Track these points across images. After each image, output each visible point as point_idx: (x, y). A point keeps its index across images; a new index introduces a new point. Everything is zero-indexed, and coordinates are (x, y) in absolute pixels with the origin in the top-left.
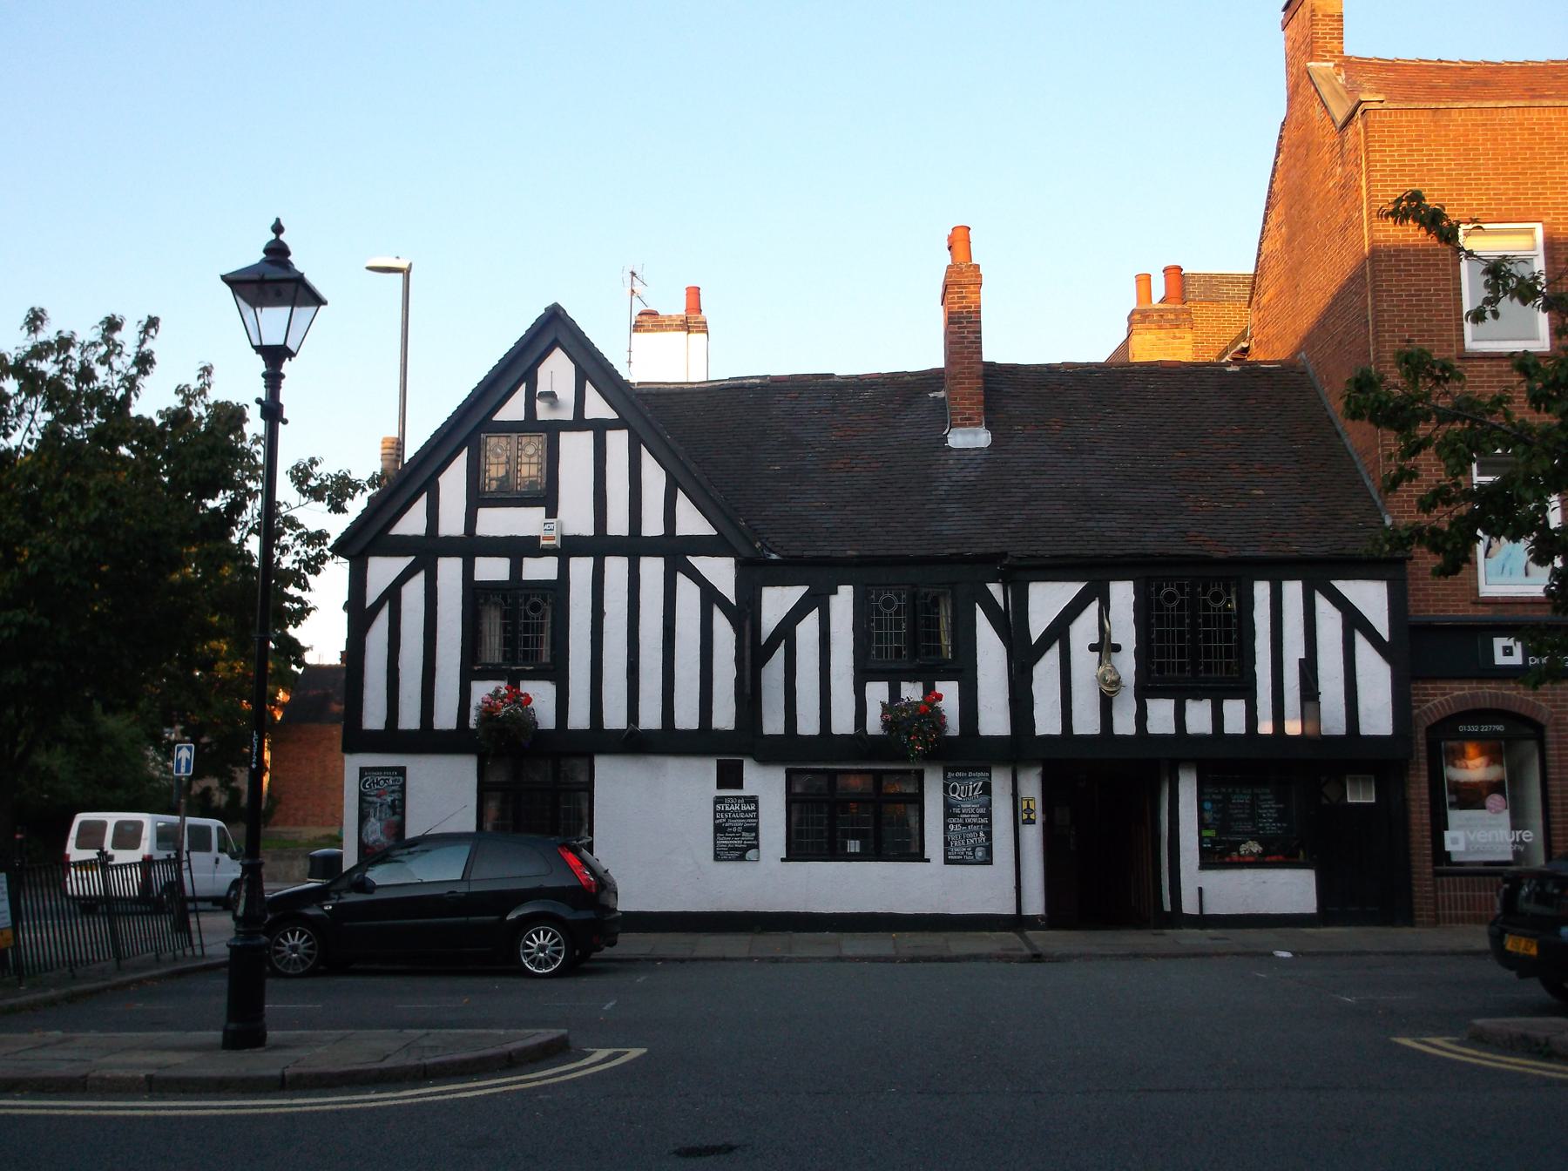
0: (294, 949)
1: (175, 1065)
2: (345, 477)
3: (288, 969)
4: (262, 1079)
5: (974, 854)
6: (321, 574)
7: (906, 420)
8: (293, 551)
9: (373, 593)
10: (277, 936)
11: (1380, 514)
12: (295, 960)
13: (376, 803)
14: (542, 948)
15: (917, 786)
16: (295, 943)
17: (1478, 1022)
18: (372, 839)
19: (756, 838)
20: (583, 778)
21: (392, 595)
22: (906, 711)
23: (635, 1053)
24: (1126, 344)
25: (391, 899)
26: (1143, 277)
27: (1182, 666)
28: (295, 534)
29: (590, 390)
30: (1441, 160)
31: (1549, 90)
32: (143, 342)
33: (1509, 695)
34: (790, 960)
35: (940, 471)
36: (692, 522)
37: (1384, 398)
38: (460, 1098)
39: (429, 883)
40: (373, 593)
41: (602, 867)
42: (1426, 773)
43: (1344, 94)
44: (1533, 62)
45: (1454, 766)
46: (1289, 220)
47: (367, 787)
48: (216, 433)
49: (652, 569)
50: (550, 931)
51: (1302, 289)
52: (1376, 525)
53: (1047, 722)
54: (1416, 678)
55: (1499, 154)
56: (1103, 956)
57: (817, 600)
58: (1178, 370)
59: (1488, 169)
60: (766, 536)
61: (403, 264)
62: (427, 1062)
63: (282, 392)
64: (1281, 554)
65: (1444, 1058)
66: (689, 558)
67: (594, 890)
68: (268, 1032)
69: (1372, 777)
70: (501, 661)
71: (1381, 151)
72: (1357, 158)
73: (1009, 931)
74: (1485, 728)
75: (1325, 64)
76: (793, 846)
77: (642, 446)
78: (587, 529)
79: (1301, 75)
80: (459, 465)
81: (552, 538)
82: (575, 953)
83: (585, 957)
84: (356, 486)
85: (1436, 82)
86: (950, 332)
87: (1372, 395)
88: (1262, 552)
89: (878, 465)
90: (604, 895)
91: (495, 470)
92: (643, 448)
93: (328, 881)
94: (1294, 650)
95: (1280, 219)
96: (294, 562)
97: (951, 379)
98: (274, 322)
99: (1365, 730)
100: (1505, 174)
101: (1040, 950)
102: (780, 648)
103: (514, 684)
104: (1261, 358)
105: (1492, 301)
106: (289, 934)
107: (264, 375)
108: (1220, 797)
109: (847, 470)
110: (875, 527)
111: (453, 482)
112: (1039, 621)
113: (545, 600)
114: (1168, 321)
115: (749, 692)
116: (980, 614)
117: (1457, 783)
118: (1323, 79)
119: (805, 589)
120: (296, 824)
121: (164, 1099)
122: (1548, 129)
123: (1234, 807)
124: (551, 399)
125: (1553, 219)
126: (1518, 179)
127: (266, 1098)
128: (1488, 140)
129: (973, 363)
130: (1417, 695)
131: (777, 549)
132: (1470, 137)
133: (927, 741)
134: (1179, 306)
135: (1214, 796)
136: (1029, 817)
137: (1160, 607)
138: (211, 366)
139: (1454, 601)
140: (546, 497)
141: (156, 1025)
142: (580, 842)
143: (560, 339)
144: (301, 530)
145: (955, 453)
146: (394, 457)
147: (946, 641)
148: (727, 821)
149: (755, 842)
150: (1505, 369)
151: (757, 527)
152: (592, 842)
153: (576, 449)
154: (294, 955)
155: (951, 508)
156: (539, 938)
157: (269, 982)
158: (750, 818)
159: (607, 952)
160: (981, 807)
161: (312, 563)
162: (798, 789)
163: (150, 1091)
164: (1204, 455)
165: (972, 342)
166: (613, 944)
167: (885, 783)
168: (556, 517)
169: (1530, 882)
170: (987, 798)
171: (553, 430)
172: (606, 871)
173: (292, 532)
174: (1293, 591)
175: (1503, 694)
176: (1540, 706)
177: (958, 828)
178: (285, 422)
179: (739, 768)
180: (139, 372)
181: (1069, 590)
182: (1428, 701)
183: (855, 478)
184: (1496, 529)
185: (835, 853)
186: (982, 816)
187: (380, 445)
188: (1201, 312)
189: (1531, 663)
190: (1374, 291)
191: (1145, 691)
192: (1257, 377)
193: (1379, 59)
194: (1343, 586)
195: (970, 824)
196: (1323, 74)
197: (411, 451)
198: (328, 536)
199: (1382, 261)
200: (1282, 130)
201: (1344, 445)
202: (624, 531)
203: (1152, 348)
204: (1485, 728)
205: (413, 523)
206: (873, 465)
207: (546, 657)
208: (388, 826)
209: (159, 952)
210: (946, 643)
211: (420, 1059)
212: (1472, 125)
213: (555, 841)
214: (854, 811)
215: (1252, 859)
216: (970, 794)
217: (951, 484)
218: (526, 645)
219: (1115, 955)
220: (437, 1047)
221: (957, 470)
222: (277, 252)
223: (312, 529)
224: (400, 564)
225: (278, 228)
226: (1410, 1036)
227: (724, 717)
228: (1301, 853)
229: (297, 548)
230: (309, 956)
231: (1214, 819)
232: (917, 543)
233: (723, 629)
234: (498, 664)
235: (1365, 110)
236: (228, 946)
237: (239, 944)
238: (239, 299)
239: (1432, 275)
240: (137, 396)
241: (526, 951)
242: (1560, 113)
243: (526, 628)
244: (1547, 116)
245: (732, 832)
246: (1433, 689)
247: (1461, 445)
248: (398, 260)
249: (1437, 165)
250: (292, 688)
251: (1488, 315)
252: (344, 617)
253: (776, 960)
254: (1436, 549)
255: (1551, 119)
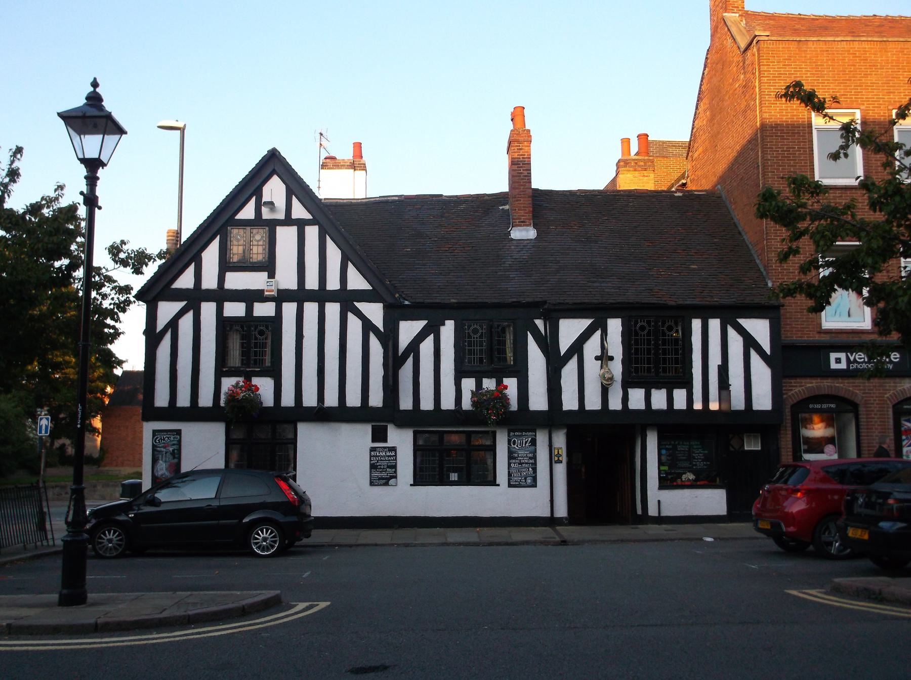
0: (110, 541)
1: (26, 617)
2: (143, 252)
3: (106, 553)
4: (82, 626)
5: (526, 482)
6: (127, 312)
7: (486, 222)
8: (110, 298)
9: (161, 324)
10: (100, 533)
11: (765, 280)
12: (111, 547)
13: (163, 451)
14: (265, 539)
15: (492, 440)
16: (111, 537)
17: (837, 580)
18: (160, 473)
19: (395, 472)
20: (291, 436)
21: (173, 324)
22: (486, 395)
23: (323, 605)
24: (614, 181)
25: (181, 509)
26: (625, 140)
27: (649, 370)
28: (111, 286)
29: (295, 201)
30: (802, 71)
31: (863, 32)
32: (12, 162)
33: (838, 387)
34: (415, 545)
35: (507, 252)
36: (357, 281)
37: (781, 204)
38: (211, 637)
39: (194, 500)
40: (161, 324)
41: (301, 490)
42: (790, 432)
43: (746, 33)
44: (853, 16)
45: (806, 428)
46: (711, 108)
47: (157, 442)
48: (59, 220)
49: (333, 310)
50: (270, 529)
51: (719, 148)
52: (762, 286)
53: (570, 402)
54: (785, 377)
55: (836, 68)
56: (603, 541)
57: (433, 329)
58: (646, 195)
59: (830, 77)
60: (402, 290)
61: (180, 125)
62: (190, 613)
63: (98, 189)
64: (707, 302)
65: (819, 603)
66: (356, 303)
67: (297, 504)
68: (89, 595)
69: (759, 434)
70: (240, 365)
71: (768, 65)
72: (753, 69)
73: (546, 526)
74: (825, 406)
75: (734, 15)
76: (418, 477)
77: (327, 235)
78: (293, 285)
79: (719, 21)
80: (214, 246)
81: (272, 291)
82: (285, 542)
83: (291, 544)
84: (150, 258)
85: (797, 27)
86: (513, 170)
87: (774, 203)
88: (696, 302)
89: (469, 248)
90: (303, 506)
91: (236, 251)
92: (328, 237)
93: (132, 499)
94: (715, 360)
95: (706, 107)
96: (110, 304)
97: (513, 198)
98: (92, 144)
99: (756, 407)
100: (839, 80)
101: (566, 538)
102: (410, 358)
103: (248, 379)
104: (694, 189)
105: (845, 147)
106: (107, 532)
107: (85, 178)
108: (671, 447)
109: (450, 251)
110: (468, 285)
111: (211, 256)
112: (565, 343)
113: (267, 327)
114: (639, 166)
115: (392, 384)
116: (530, 338)
117: (808, 438)
118: (733, 23)
119: (425, 322)
120: (117, 466)
121: (18, 639)
122: (864, 54)
123: (679, 452)
124: (271, 206)
125: (867, 107)
126: (846, 83)
127: (85, 638)
128: (830, 60)
129: (526, 188)
130: (786, 386)
131: (410, 298)
132: (819, 58)
133: (498, 414)
134: (646, 158)
135: (667, 446)
136: (558, 458)
137: (636, 334)
138: (65, 186)
139: (807, 331)
140: (269, 267)
141: (20, 590)
142: (288, 475)
143: (276, 169)
144: (116, 284)
145: (515, 242)
146: (175, 241)
147: (510, 355)
148: (378, 462)
149: (395, 475)
150: (837, 195)
151: (396, 285)
152: (296, 474)
153: (286, 237)
154: (111, 545)
155: (512, 274)
156: (263, 533)
157: (90, 563)
158: (392, 460)
159: (305, 541)
160: (530, 453)
161: (122, 306)
162: (421, 442)
163: (9, 634)
164: (662, 244)
165: (526, 176)
166: (308, 536)
167: (472, 439)
168: (274, 278)
169: (863, 495)
170: (533, 448)
171: (272, 225)
172: (304, 492)
173: (109, 285)
174: (715, 325)
175: (835, 386)
176: (856, 393)
177: (516, 466)
178: (100, 208)
179: (385, 430)
180: (10, 181)
181: (583, 324)
182: (791, 390)
183: (456, 257)
184: (847, 283)
185: (443, 481)
186: (530, 458)
187: (166, 235)
188: (659, 163)
189: (851, 368)
190: (762, 148)
191: (628, 383)
192: (692, 199)
193: (765, 13)
194: (744, 322)
195: (524, 463)
196: (732, 20)
197: (185, 237)
198: (132, 289)
199: (768, 130)
200: (707, 54)
201: (744, 239)
202: (316, 287)
203: (630, 182)
204: (825, 406)
205: (186, 281)
206: (466, 249)
207: (268, 363)
208: (170, 466)
209: (26, 544)
210: (510, 355)
211: (185, 611)
212: (820, 51)
213: (273, 474)
214: (454, 455)
215: (689, 483)
216: (524, 446)
217: (513, 260)
218: (256, 355)
219: (610, 541)
220: (197, 603)
221: (517, 252)
222: (94, 99)
223: (122, 284)
224: (178, 306)
225: (95, 84)
226: (795, 589)
227: (376, 399)
228: (718, 480)
229: (113, 296)
230: (120, 545)
231: (668, 460)
232: (493, 295)
233: (375, 345)
234: (238, 367)
235: (759, 41)
236: (62, 540)
237: (69, 539)
238: (69, 128)
239: (796, 139)
240: (9, 196)
241: (254, 541)
242: (871, 45)
243: (256, 346)
244: (863, 46)
245: (381, 468)
246: (795, 383)
247: (827, 233)
248: (177, 122)
249: (800, 74)
250: (115, 385)
251: (842, 155)
252: (143, 338)
253: (407, 545)
254: (810, 296)
255: (866, 48)
